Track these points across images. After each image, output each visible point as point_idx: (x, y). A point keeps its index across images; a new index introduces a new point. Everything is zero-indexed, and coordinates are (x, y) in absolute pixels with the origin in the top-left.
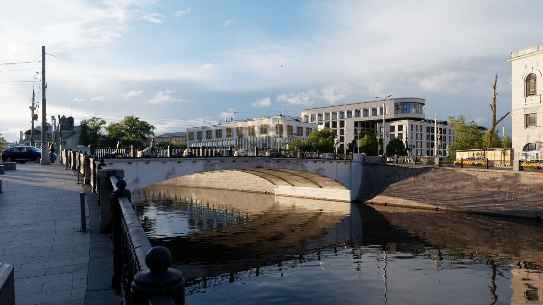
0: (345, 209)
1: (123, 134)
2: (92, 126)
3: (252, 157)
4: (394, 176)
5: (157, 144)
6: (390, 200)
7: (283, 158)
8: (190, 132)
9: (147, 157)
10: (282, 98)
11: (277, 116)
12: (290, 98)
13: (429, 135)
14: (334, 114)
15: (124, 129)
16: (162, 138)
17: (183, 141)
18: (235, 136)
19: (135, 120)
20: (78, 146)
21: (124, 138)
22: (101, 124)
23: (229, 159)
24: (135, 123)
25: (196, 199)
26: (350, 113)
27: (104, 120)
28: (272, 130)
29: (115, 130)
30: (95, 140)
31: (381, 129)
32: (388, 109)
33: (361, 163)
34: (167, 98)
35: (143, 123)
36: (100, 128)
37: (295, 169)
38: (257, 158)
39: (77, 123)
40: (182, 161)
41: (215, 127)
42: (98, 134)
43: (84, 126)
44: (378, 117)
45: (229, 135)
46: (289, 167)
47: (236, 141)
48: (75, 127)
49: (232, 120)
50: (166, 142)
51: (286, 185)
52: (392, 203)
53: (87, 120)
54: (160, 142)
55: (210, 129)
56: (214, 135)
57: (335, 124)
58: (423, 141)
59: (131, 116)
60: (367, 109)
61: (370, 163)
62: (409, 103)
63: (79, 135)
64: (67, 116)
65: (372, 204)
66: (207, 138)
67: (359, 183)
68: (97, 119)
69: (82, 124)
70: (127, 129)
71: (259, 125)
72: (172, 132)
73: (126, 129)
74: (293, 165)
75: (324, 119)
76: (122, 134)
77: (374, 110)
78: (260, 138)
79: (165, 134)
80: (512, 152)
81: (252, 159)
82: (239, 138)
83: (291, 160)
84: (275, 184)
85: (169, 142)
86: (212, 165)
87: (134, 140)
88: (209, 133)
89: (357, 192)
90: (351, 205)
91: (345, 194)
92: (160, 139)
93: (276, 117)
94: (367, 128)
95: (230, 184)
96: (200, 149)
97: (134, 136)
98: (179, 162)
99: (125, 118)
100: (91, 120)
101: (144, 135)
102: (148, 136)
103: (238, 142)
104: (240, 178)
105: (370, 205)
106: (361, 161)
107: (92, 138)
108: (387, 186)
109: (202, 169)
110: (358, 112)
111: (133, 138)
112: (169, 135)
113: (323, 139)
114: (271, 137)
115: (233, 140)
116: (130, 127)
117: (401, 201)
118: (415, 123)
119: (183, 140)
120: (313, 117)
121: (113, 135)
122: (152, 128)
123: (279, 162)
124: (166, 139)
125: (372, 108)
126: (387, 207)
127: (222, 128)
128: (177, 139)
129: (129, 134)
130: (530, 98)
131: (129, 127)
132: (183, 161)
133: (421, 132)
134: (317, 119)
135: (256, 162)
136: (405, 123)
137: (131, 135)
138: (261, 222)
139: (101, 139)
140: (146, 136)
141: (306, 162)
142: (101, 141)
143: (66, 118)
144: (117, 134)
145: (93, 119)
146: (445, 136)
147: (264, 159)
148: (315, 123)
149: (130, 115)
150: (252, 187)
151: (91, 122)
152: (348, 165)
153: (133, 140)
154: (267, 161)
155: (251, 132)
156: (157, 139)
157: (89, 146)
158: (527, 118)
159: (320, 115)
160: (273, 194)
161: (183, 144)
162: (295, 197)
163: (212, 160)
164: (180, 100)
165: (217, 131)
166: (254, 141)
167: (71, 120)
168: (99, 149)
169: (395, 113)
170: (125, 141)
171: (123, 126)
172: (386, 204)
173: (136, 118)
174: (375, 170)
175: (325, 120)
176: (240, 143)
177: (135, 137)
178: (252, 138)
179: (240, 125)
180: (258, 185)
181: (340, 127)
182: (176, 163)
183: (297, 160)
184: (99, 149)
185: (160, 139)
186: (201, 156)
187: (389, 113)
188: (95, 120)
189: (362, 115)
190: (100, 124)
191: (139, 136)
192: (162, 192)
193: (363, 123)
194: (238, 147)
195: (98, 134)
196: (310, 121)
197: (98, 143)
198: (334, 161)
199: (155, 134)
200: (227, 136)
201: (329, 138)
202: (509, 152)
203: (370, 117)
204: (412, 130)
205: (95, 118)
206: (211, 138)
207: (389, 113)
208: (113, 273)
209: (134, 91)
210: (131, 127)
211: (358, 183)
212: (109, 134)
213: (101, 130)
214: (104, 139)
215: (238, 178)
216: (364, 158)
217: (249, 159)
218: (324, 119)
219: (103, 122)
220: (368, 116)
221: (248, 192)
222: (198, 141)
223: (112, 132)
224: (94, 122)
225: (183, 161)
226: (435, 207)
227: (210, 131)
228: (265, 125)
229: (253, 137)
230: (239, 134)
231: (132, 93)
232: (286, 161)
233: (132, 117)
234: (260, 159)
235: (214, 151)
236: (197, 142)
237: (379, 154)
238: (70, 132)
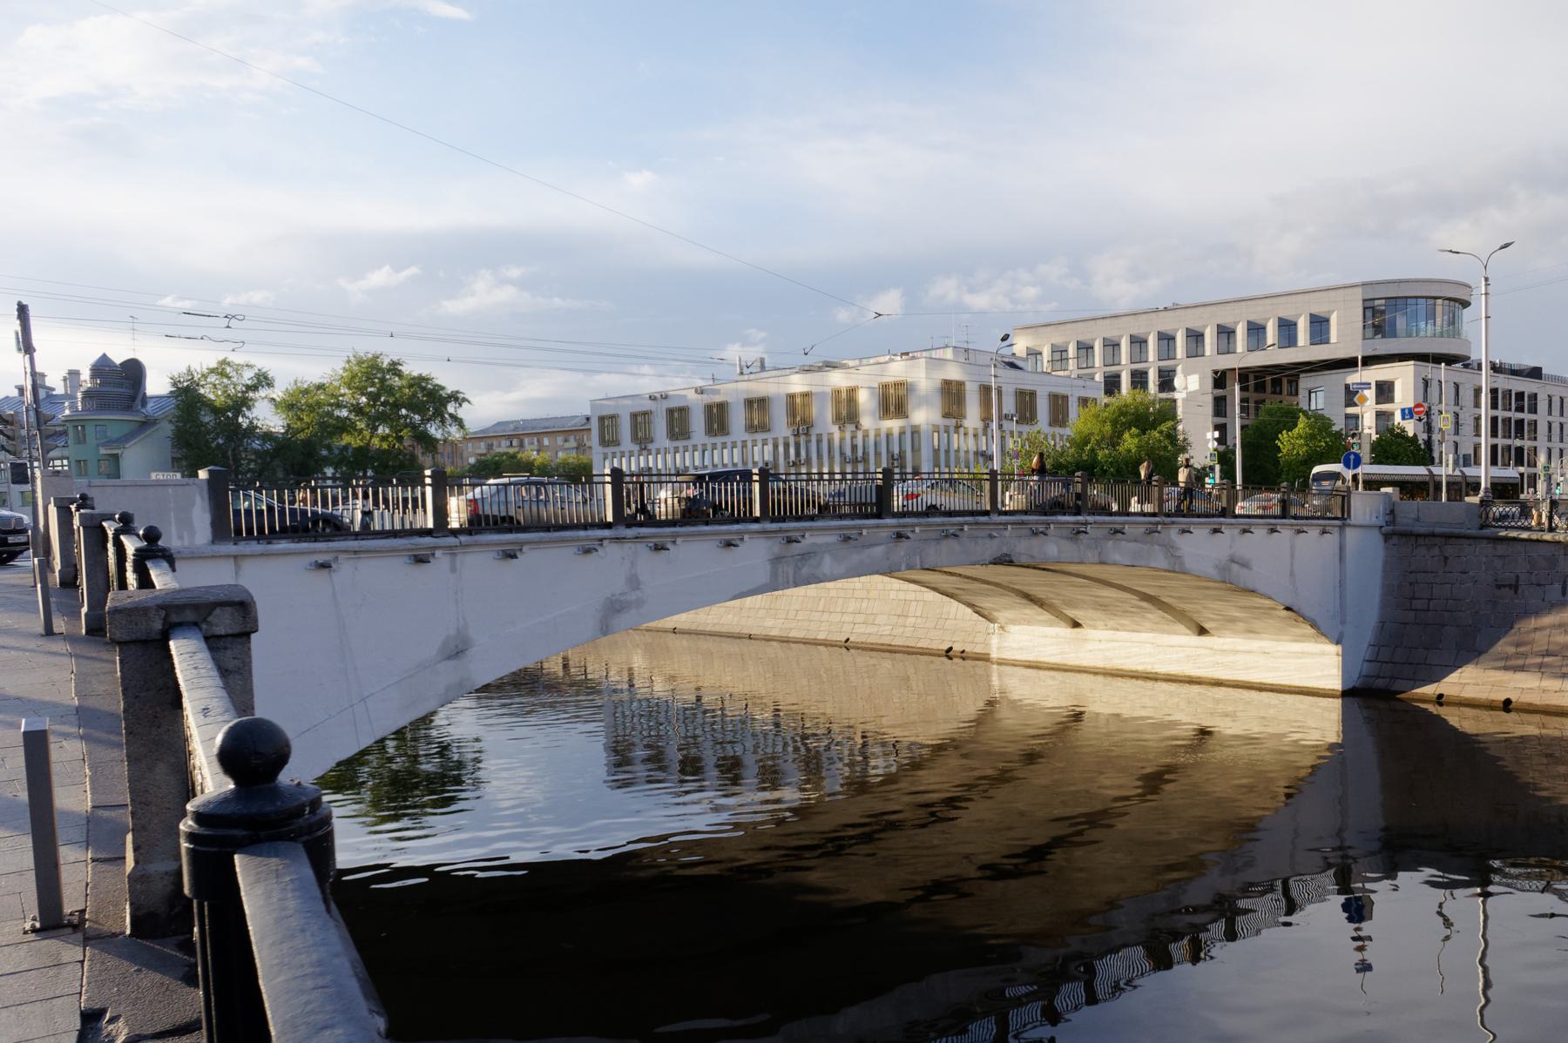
1: (344, 427)
2: (217, 396)
3: (972, 513)
4: (1539, 585)
5: (472, 460)
6: (1526, 686)
7: (1098, 518)
8: (605, 413)
9: (505, 524)
10: (947, 289)
11: (940, 348)
12: (972, 290)
13: (1510, 418)
14: (1138, 342)
15: (345, 407)
16: (489, 441)
17: (567, 449)
18: (782, 428)
19: (389, 371)
20: (154, 476)
21: (346, 439)
22: (254, 388)
23: (878, 527)
24: (387, 383)
26: (1195, 337)
27: (264, 370)
28: (925, 401)
29: (311, 408)
30: (234, 450)
31: (1313, 395)
32: (1338, 325)
33: (1381, 532)
34: (507, 294)
35: (419, 382)
36: (251, 403)
37: (1143, 563)
38: (996, 518)
39: (157, 385)
40: (674, 542)
42: (245, 425)
43: (187, 396)
44: (1304, 350)
45: (756, 423)
46: (1117, 557)
48: (152, 398)
49: (763, 368)
50: (506, 454)
53: (199, 370)
54: (481, 455)
55: (682, 404)
56: (698, 423)
57: (1139, 379)
58: (1464, 438)
59: (370, 356)
60: (1322, 315)
61: (1422, 530)
62: (1413, 301)
63: (167, 429)
64: (118, 358)
65: (1441, 704)
67: (1371, 617)
68: (238, 368)
69: (178, 388)
70: (358, 404)
71: (877, 386)
72: (526, 418)
73: (352, 405)
74: (1132, 545)
75: (1098, 361)
76: (340, 425)
77: (1287, 329)
78: (877, 435)
79: (499, 424)
81: (977, 523)
82: (797, 435)
83: (1127, 527)
85: (518, 452)
86: (805, 556)
87: (385, 446)
88: (678, 420)
89: (1363, 650)
90: (1344, 706)
92: (482, 445)
93: (933, 352)
94: (1256, 394)
95: (791, 615)
96: (751, 481)
97: (387, 431)
98: (659, 548)
99: (349, 362)
100: (212, 371)
101: (426, 429)
102: (440, 431)
103: (792, 451)
105: (1432, 708)
106: (1381, 522)
107: (221, 441)
109: (763, 576)
110: (1226, 333)
111: (384, 438)
113: (1137, 436)
114: (924, 428)
116: (370, 395)
118: (1429, 369)
119: (567, 445)
120: (1060, 353)
121: (303, 430)
122: (456, 399)
123: (1082, 536)
125: (1280, 319)
126: (1513, 715)
128: (546, 442)
129: (368, 425)
132: (679, 540)
133: (1455, 405)
134: (1072, 364)
135: (991, 537)
136: (1403, 378)
137: (375, 428)
138: (937, 781)
139: (256, 444)
140: (434, 430)
141: (1184, 531)
142: (256, 452)
143: (116, 366)
145: (221, 370)
146: (1536, 421)
147: (1023, 523)
148: (1069, 377)
150: (887, 630)
151: (213, 378)
152: (1332, 539)
153: (381, 446)
154: (1035, 534)
155: (844, 413)
156: (470, 445)
157: (203, 474)
159: (1085, 348)
160: (984, 658)
161: (571, 460)
163: (807, 535)
164: (557, 301)
165: (709, 408)
166: (854, 447)
167: (133, 372)
168: (259, 491)
170: (350, 450)
171: (343, 395)
172: (1507, 705)
173: (389, 364)
174: (1446, 558)
175: (1104, 366)
177: (388, 436)
178: (848, 436)
179: (797, 384)
180: (911, 621)
182: (642, 549)
183: (1150, 523)
184: (259, 491)
185: (482, 445)
186: (757, 513)
187: (1345, 338)
188: (228, 370)
190: (249, 388)
191: (405, 433)
193: (1245, 375)
194: (793, 470)
195: (245, 425)
197: (246, 459)
198: (1285, 525)
199: (467, 424)
200: (751, 428)
201: (1161, 432)
205: (229, 364)
207: (1345, 338)
209: (387, 268)
210: (374, 398)
211: (1368, 613)
212: (288, 425)
213: (254, 410)
214: (268, 446)
216: (1392, 512)
217: (962, 524)
218: (1098, 361)
219: (263, 380)
220: (1327, 342)
221: (872, 650)
222: (636, 448)
223: (301, 420)
224: (225, 380)
225: (679, 540)
228: (898, 385)
229: (854, 429)
230: (798, 419)
231: (380, 277)
232: (1106, 531)
233: (376, 357)
234: (1006, 524)
235: (802, 490)
236: (631, 454)
238: (131, 418)
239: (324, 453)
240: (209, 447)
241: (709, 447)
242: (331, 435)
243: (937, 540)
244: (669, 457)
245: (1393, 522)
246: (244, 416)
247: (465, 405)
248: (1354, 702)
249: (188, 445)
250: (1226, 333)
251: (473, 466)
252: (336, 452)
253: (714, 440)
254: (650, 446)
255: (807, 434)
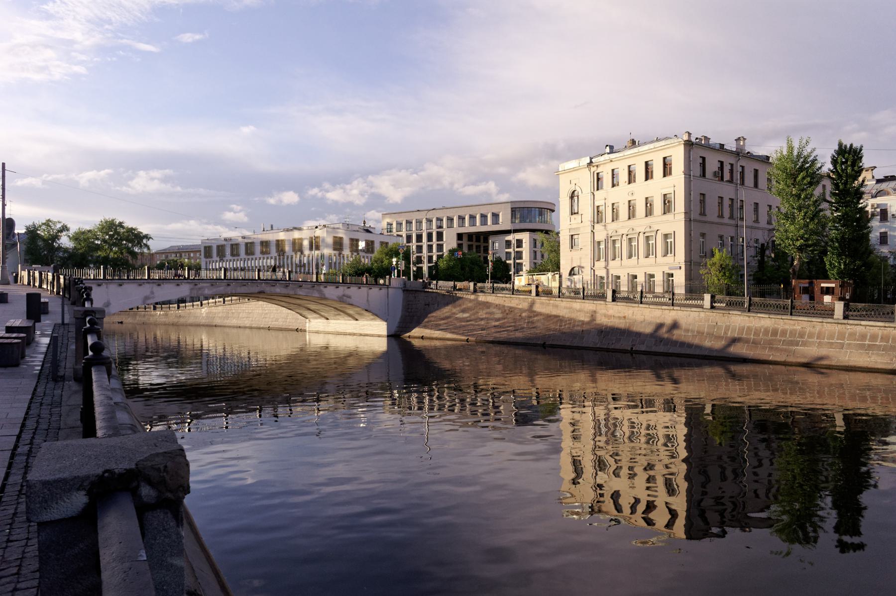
0: (381, 345)
1: (98, 248)
6: (427, 332)
8: (207, 245)
16: (167, 254)
19: (118, 226)
25: (209, 342)
26: (450, 220)
28: (327, 246)
29: (85, 240)
30: (51, 256)
35: (131, 230)
38: (259, 281)
41: (244, 238)
43: (32, 233)
44: (490, 227)
47: (275, 259)
50: (173, 260)
51: (319, 318)
52: (428, 336)
57: (419, 238)
66: (232, 255)
68: (55, 223)
79: (171, 247)
80: (560, 277)
82: (279, 256)
84: (307, 318)
87: (116, 256)
89: (396, 324)
91: (380, 327)
92: (164, 256)
98: (159, 285)
99: (101, 222)
100: (43, 224)
104: (267, 311)
105: (408, 339)
106: (402, 286)
107: (46, 253)
108: (426, 316)
110: (462, 219)
111: (115, 253)
112: (179, 249)
115: (272, 258)
116: (110, 236)
117: (437, 334)
118: (540, 236)
124: (173, 255)
125: (481, 214)
127: (255, 241)
128: (192, 255)
130: (574, 216)
131: (107, 237)
136: (525, 237)
139: (61, 254)
140: (136, 250)
141: (325, 287)
142: (60, 257)
144: (89, 247)
145: (48, 223)
149: (109, 217)
150: (281, 323)
151: (44, 227)
152: (384, 291)
158: (572, 239)
162: (329, 333)
165: (247, 244)
169: (512, 222)
172: (422, 338)
176: (282, 264)
177: (117, 252)
179: (282, 236)
181: (438, 241)
185: (164, 256)
188: (50, 224)
189: (467, 224)
192: (158, 334)
193: (470, 236)
196: (394, 230)
200: (262, 253)
202: (557, 276)
203: (479, 228)
204: (535, 247)
206: (253, 253)
207: (505, 222)
208: (82, 407)
214: (66, 255)
215: (264, 312)
219: (65, 228)
223: (80, 244)
226: (467, 338)
227: (237, 245)
236: (217, 261)
237: (403, 276)
239: (90, 258)
240: (41, 255)
241: (247, 259)
242: (92, 251)
243: (240, 286)
244: (217, 264)
245: (405, 287)
246: (56, 242)
247: (151, 240)
248: (393, 339)
249: (32, 254)
250: (462, 219)
251: (158, 265)
252: (94, 258)
253: (234, 258)
254: (224, 259)
255: (283, 255)
